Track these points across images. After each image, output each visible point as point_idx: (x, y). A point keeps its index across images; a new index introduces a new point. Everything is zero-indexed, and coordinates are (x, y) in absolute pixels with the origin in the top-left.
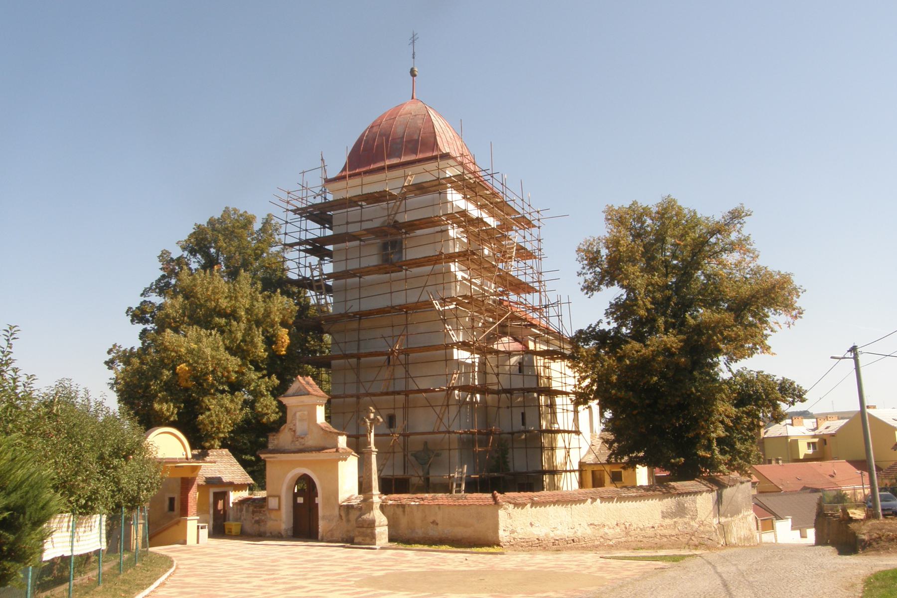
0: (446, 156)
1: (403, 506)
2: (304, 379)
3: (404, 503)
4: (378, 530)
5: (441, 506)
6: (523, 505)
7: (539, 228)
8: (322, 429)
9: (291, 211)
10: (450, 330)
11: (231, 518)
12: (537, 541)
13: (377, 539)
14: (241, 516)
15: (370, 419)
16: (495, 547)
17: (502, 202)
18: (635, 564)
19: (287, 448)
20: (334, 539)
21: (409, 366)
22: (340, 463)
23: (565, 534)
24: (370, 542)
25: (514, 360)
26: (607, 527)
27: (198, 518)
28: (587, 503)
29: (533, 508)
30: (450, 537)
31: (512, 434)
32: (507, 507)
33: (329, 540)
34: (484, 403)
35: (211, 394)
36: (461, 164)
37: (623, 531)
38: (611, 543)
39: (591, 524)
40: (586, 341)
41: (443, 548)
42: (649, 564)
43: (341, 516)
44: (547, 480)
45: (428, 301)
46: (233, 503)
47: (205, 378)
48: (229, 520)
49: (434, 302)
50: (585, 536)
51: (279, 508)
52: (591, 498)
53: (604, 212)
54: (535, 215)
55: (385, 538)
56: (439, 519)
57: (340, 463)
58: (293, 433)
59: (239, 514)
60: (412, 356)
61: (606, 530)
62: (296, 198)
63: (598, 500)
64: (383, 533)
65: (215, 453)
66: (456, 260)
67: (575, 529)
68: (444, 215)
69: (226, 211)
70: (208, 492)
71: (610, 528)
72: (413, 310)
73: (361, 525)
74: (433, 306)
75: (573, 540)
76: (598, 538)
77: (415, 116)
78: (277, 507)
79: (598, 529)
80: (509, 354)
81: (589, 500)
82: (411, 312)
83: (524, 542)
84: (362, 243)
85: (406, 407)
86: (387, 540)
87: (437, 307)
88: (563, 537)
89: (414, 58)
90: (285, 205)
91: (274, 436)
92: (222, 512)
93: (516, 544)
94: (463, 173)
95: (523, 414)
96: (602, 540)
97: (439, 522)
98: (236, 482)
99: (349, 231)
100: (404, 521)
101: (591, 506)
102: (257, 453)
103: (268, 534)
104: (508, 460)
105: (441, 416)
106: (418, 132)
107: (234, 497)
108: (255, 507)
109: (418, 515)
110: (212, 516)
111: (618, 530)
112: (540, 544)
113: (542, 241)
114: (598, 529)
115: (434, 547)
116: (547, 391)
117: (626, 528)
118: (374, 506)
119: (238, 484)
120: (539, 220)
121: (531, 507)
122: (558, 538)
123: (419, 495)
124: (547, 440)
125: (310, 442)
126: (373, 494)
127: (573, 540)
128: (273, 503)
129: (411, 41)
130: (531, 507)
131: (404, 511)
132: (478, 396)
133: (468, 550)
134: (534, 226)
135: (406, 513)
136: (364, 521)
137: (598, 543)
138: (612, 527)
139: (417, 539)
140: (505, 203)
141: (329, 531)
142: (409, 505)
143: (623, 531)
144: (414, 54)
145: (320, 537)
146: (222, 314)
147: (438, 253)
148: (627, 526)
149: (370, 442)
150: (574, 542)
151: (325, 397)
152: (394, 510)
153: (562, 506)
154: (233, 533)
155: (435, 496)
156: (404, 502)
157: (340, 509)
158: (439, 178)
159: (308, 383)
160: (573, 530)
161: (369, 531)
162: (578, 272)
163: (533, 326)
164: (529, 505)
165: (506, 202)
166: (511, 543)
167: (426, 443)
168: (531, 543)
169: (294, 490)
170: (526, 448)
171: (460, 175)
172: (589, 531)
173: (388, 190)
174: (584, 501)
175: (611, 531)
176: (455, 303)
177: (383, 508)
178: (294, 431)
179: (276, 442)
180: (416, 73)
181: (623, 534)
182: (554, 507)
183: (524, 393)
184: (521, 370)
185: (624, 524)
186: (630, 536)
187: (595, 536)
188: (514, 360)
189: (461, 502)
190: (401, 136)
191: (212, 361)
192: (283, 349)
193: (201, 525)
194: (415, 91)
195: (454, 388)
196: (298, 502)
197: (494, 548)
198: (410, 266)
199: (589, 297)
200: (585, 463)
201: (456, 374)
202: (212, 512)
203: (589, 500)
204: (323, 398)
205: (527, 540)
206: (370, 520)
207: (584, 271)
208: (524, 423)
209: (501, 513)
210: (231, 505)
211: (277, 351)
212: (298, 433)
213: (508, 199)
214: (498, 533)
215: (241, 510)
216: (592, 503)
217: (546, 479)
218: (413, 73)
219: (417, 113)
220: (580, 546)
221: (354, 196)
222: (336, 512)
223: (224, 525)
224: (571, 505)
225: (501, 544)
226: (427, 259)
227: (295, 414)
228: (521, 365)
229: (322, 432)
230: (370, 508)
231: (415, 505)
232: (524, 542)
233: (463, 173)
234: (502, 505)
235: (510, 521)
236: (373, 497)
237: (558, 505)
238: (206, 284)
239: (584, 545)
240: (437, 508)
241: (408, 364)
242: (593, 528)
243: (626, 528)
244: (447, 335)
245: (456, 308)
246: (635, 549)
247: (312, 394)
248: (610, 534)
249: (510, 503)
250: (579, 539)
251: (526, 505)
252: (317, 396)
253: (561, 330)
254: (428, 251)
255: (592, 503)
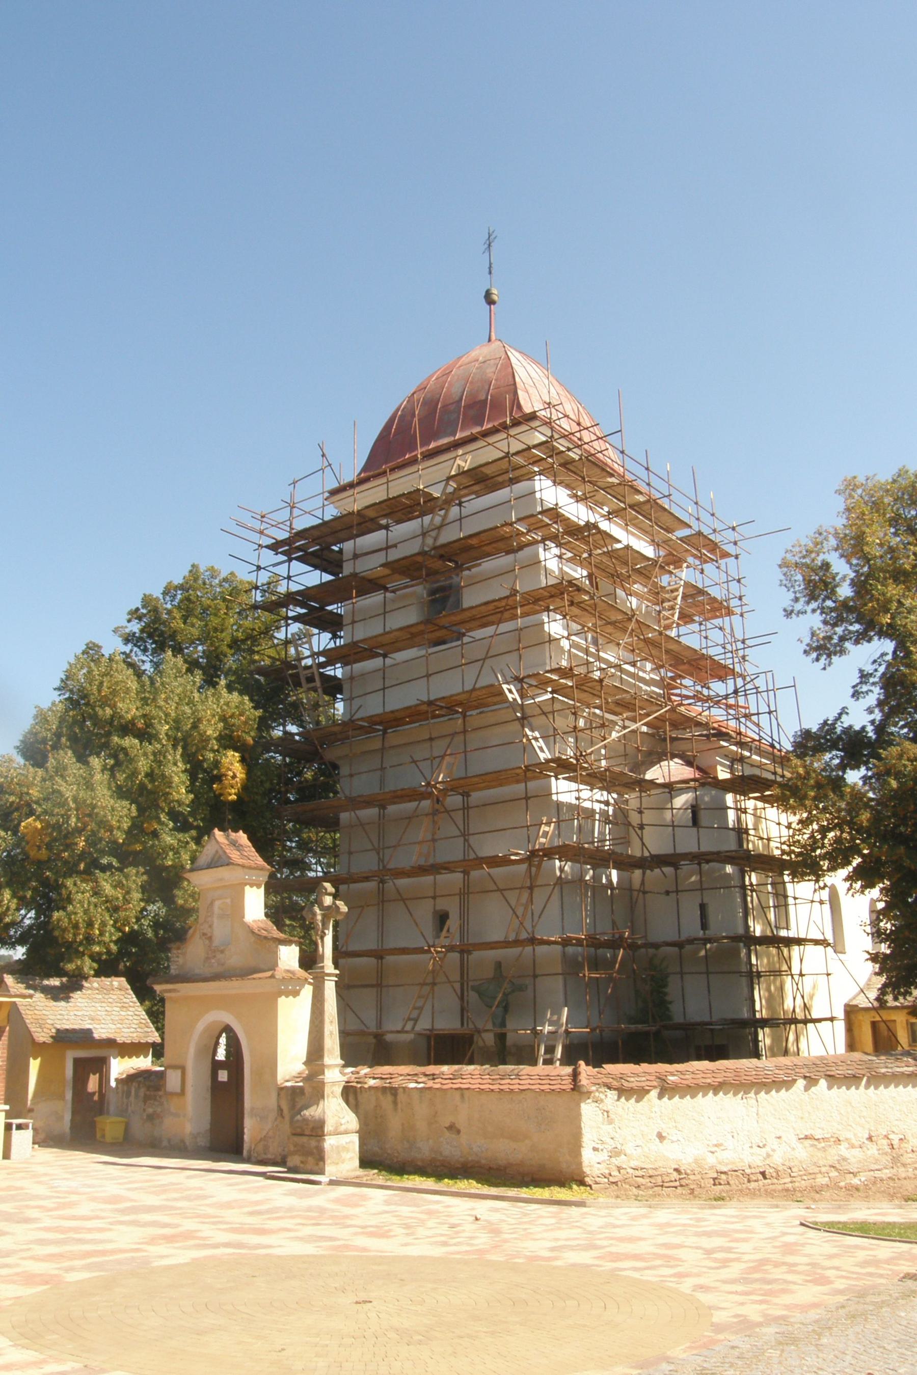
0: (533, 416)
1: (393, 1091)
2: (227, 837)
3: (395, 1085)
4: (329, 1143)
5: (466, 1093)
6: (640, 1093)
7: (737, 557)
8: (253, 933)
9: (267, 547)
10: (536, 739)
11: (112, 1108)
12: (675, 1175)
13: (328, 1161)
14: (127, 1105)
15: (322, 907)
16: (575, 1187)
17: (648, 501)
18: (862, 1255)
19: (197, 971)
20: (269, 1156)
21: (471, 811)
22: (282, 1001)
23: (742, 1160)
24: (316, 1168)
25: (681, 801)
26: (844, 1145)
27: (7, 1107)
28: (794, 1089)
29: (665, 1099)
30: (483, 1162)
31: (679, 945)
32: (602, 1096)
33: (260, 1158)
34: (625, 887)
35: (79, 873)
36: (548, 423)
37: (886, 1154)
38: (856, 1181)
39: (806, 1138)
40: (819, 749)
41: (463, 1185)
42: (900, 1256)
43: (280, 1110)
44: (768, 1041)
45: (492, 686)
46: (116, 1080)
47: (68, 841)
48: (108, 1113)
49: (505, 687)
50: (792, 1164)
51: (183, 1092)
52: (805, 1077)
53: (839, 492)
54: (730, 535)
55: (351, 1159)
56: (461, 1121)
57: (282, 1001)
58: (207, 942)
59: (125, 1100)
60: (476, 797)
61: (843, 1149)
62: (274, 523)
63: (823, 1083)
64: (346, 1149)
65: (95, 985)
66: (551, 608)
67: (768, 1149)
68: (519, 520)
69: (194, 569)
70: (63, 1058)
71: (853, 1147)
72: (477, 708)
73: (299, 1130)
74: (501, 693)
75: (763, 1174)
76: (824, 1169)
77: (484, 362)
78: (178, 1090)
79: (824, 1149)
80: (670, 788)
81: (801, 1083)
82: (474, 712)
83: (643, 1177)
84: (388, 595)
85: (465, 893)
86: (357, 1163)
87: (510, 697)
88: (739, 1166)
89: (490, 273)
90: (255, 537)
91: (178, 948)
92: (96, 1098)
93: (625, 1180)
94: (552, 437)
95: (703, 907)
96: (834, 1174)
97: (462, 1128)
98: (120, 1040)
99: (357, 571)
100: (395, 1124)
101: (805, 1096)
102: (148, 982)
103: (165, 1143)
104: (668, 998)
105: (520, 911)
106: (487, 387)
107: (119, 1067)
108: (148, 1088)
109: (421, 1110)
110: (69, 1105)
111: (872, 1150)
112: (683, 1182)
113: (742, 581)
114: (824, 1149)
115: (447, 1184)
116: (742, 859)
117: (892, 1146)
118: (327, 1090)
119: (124, 1043)
120: (735, 543)
121: (660, 1096)
122: (725, 1169)
123: (431, 1069)
124: (765, 961)
125: (234, 959)
126: (323, 1065)
127: (763, 1174)
128: (173, 1080)
129: (486, 246)
130: (660, 1096)
131: (395, 1103)
132: (614, 874)
133: (512, 1192)
134: (725, 555)
135: (399, 1105)
136: (305, 1120)
137: (825, 1181)
138: (857, 1144)
139: (419, 1163)
140: (652, 503)
141: (261, 1140)
142: (405, 1089)
143: (886, 1154)
144: (490, 267)
145: (245, 1153)
146: (127, 729)
147: (508, 593)
148: (896, 1143)
149: (323, 956)
150: (765, 1178)
151: (262, 869)
152: (377, 1099)
153: (735, 1094)
154: (108, 1139)
155: (460, 1070)
156: (397, 1082)
157: (279, 1095)
158: (508, 453)
159: (234, 843)
160: (763, 1151)
161: (313, 1143)
162: (785, 610)
163: (721, 735)
164: (654, 1093)
165: (654, 500)
166: (612, 1179)
167: (498, 965)
168: (659, 1179)
169: (215, 1052)
170: (708, 973)
171: (546, 442)
172: (802, 1153)
173: (421, 487)
174: (788, 1084)
175: (856, 1152)
176: (550, 689)
177: (350, 1093)
178: (210, 938)
179: (181, 960)
180: (495, 298)
181: (885, 1160)
182: (848, 1092)
183: (699, 864)
184: (695, 821)
185: (886, 1137)
186: (904, 1165)
187: (815, 1164)
188: (681, 801)
189: (506, 1084)
190: (457, 398)
191: (77, 810)
192: (233, 791)
193: (16, 1121)
194: (493, 330)
195: (549, 853)
196: (220, 1079)
197: (571, 1188)
198: (468, 626)
199: (824, 669)
200: (857, 1006)
201: (548, 824)
202: (69, 1095)
203: (801, 1083)
204: (261, 873)
205: (651, 1172)
206: (315, 1121)
207: (799, 606)
208: (704, 926)
209: (587, 1109)
210: (113, 1084)
211: (221, 795)
212: (216, 942)
213: (658, 495)
214: (579, 1154)
215: (128, 1094)
216: (807, 1089)
217: (765, 1037)
218: (489, 300)
219: (488, 358)
220: (780, 1187)
221: (367, 507)
222: (272, 1102)
223: (95, 1122)
224: (756, 1093)
225: (587, 1179)
226: (491, 607)
227: (212, 904)
228: (695, 809)
229: (253, 939)
230: (318, 1093)
231: (416, 1088)
232: (643, 1177)
233: (552, 437)
234: (590, 1093)
235: (609, 1128)
236: (326, 1071)
237: (725, 1094)
238: (97, 677)
239: (790, 1186)
240: (457, 1095)
241: (468, 808)
242: (812, 1146)
243: (892, 1146)
244: (528, 748)
245: (553, 697)
246: (907, 1199)
247: (233, 864)
248: (853, 1160)
249: (609, 1088)
250: (777, 1172)
251: (648, 1092)
252: (243, 866)
253: (776, 737)
254: (496, 591)
255: (807, 1089)
